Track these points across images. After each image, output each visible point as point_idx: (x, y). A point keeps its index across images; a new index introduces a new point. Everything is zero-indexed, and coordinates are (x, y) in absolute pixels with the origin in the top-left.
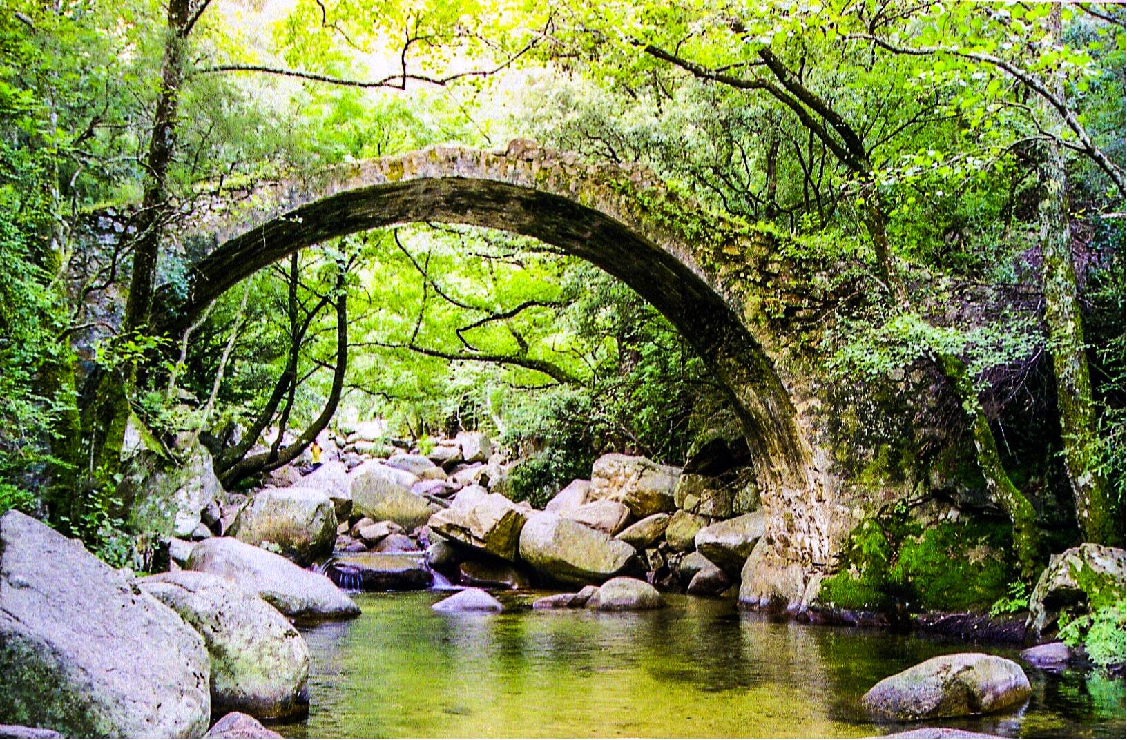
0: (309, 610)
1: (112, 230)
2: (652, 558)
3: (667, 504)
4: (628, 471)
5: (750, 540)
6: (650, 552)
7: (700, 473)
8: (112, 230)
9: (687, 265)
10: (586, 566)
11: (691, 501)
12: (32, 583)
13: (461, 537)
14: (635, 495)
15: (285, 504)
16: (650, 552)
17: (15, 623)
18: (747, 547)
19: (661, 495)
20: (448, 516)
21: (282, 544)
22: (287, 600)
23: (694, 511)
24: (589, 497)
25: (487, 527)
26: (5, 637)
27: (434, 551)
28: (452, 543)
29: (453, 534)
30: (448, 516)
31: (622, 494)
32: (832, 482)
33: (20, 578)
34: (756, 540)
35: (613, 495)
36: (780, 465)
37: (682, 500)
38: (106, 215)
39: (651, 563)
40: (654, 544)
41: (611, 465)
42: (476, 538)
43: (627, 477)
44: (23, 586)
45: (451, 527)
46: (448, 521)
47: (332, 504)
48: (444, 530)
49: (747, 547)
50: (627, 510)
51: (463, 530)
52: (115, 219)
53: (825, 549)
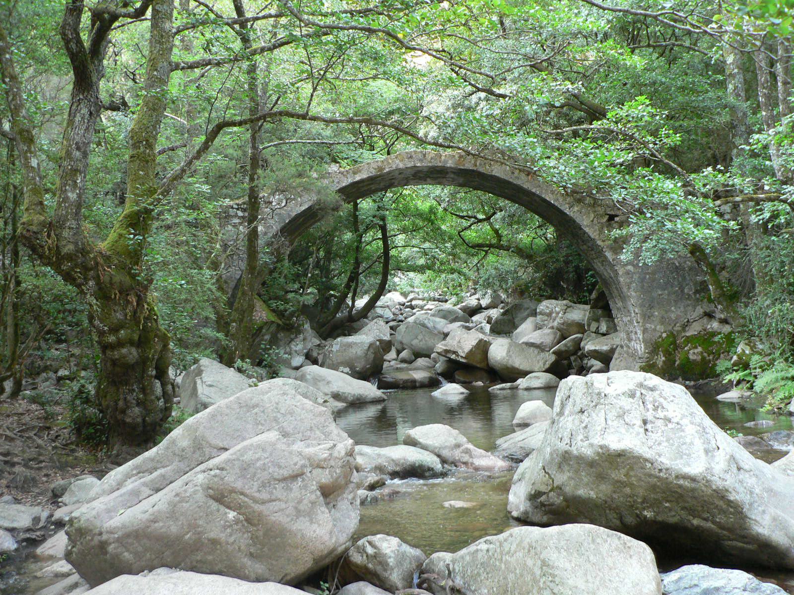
0: (358, 399)
1: (236, 216)
2: (574, 361)
3: (581, 328)
4: (557, 309)
5: (615, 346)
6: (572, 358)
7: (600, 308)
8: (236, 216)
9: (548, 199)
10: (528, 369)
11: (594, 326)
12: (214, 384)
13: (453, 357)
14: (563, 324)
15: (350, 345)
16: (572, 358)
17: (209, 400)
18: (613, 351)
19: (577, 323)
20: (445, 345)
21: (351, 369)
22: (346, 395)
23: (597, 332)
24: (538, 327)
25: (467, 350)
26: (98, 57)
27: (440, 366)
28: (450, 361)
29: (449, 355)
30: (445, 345)
31: (555, 324)
32: (643, 311)
33: (209, 383)
34: (617, 347)
35: (550, 325)
36: (620, 304)
37: (589, 326)
38: (232, 208)
39: (574, 364)
40: (575, 353)
41: (547, 307)
42: (462, 357)
43: (558, 313)
44: (211, 386)
45: (447, 351)
46: (445, 348)
47: (378, 343)
48: (443, 354)
49: (613, 351)
50: (559, 334)
51: (454, 352)
52: (238, 209)
53: (643, 349)
